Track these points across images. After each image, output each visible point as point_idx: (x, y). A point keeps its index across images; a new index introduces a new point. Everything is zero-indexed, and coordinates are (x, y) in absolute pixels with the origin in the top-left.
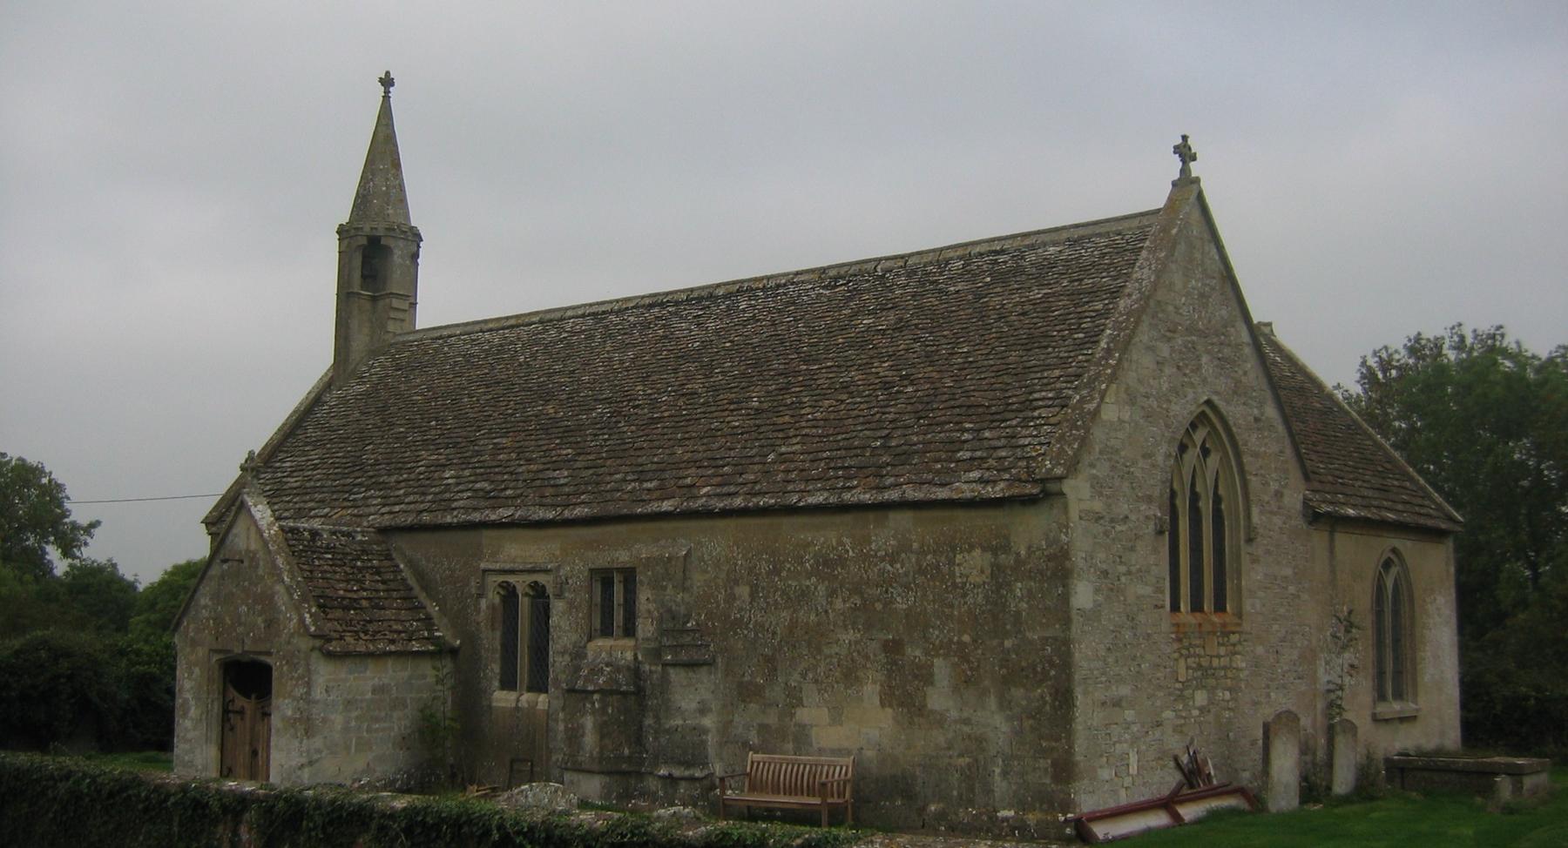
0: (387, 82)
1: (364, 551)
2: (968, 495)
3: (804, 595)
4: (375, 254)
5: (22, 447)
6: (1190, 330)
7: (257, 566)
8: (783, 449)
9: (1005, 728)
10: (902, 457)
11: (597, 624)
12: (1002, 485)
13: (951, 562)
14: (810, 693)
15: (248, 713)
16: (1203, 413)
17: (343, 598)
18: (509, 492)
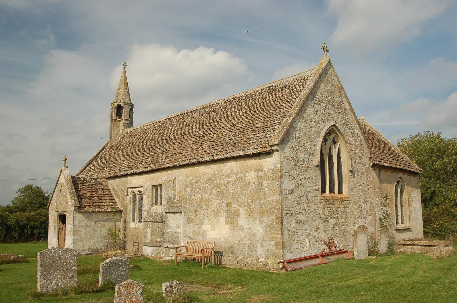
1: (100, 184)
2: (249, 153)
3: (205, 189)
4: (121, 111)
6: (327, 102)
8: (203, 146)
9: (261, 230)
10: (234, 144)
11: (154, 202)
12: (260, 149)
13: (245, 176)
14: (206, 220)
16: (333, 129)
17: (89, 196)
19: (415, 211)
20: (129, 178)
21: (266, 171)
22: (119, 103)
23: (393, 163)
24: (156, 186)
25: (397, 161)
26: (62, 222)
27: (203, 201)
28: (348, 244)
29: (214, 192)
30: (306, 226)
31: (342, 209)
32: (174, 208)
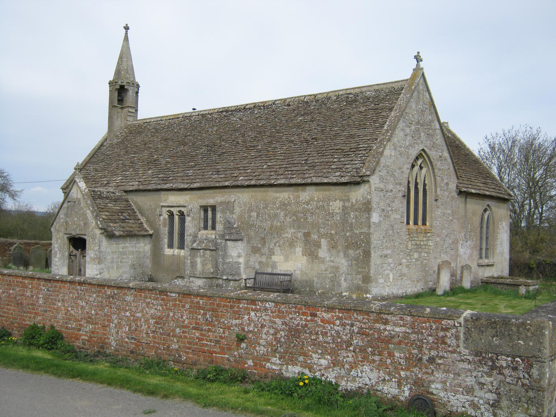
0: (127, 28)
3: (276, 216)
4: (122, 92)
7: (81, 204)
8: (270, 164)
11: (202, 225)
12: (347, 178)
13: (328, 205)
14: (277, 250)
15: (78, 256)
16: (421, 153)
18: (171, 178)
19: (501, 244)
20: (163, 194)
21: (354, 202)
22: (122, 84)
23: (482, 188)
24: (205, 209)
25: (485, 185)
26: (73, 247)
27: (273, 229)
28: (429, 280)
29: (288, 219)
30: (390, 260)
31: (425, 243)
32: (233, 234)
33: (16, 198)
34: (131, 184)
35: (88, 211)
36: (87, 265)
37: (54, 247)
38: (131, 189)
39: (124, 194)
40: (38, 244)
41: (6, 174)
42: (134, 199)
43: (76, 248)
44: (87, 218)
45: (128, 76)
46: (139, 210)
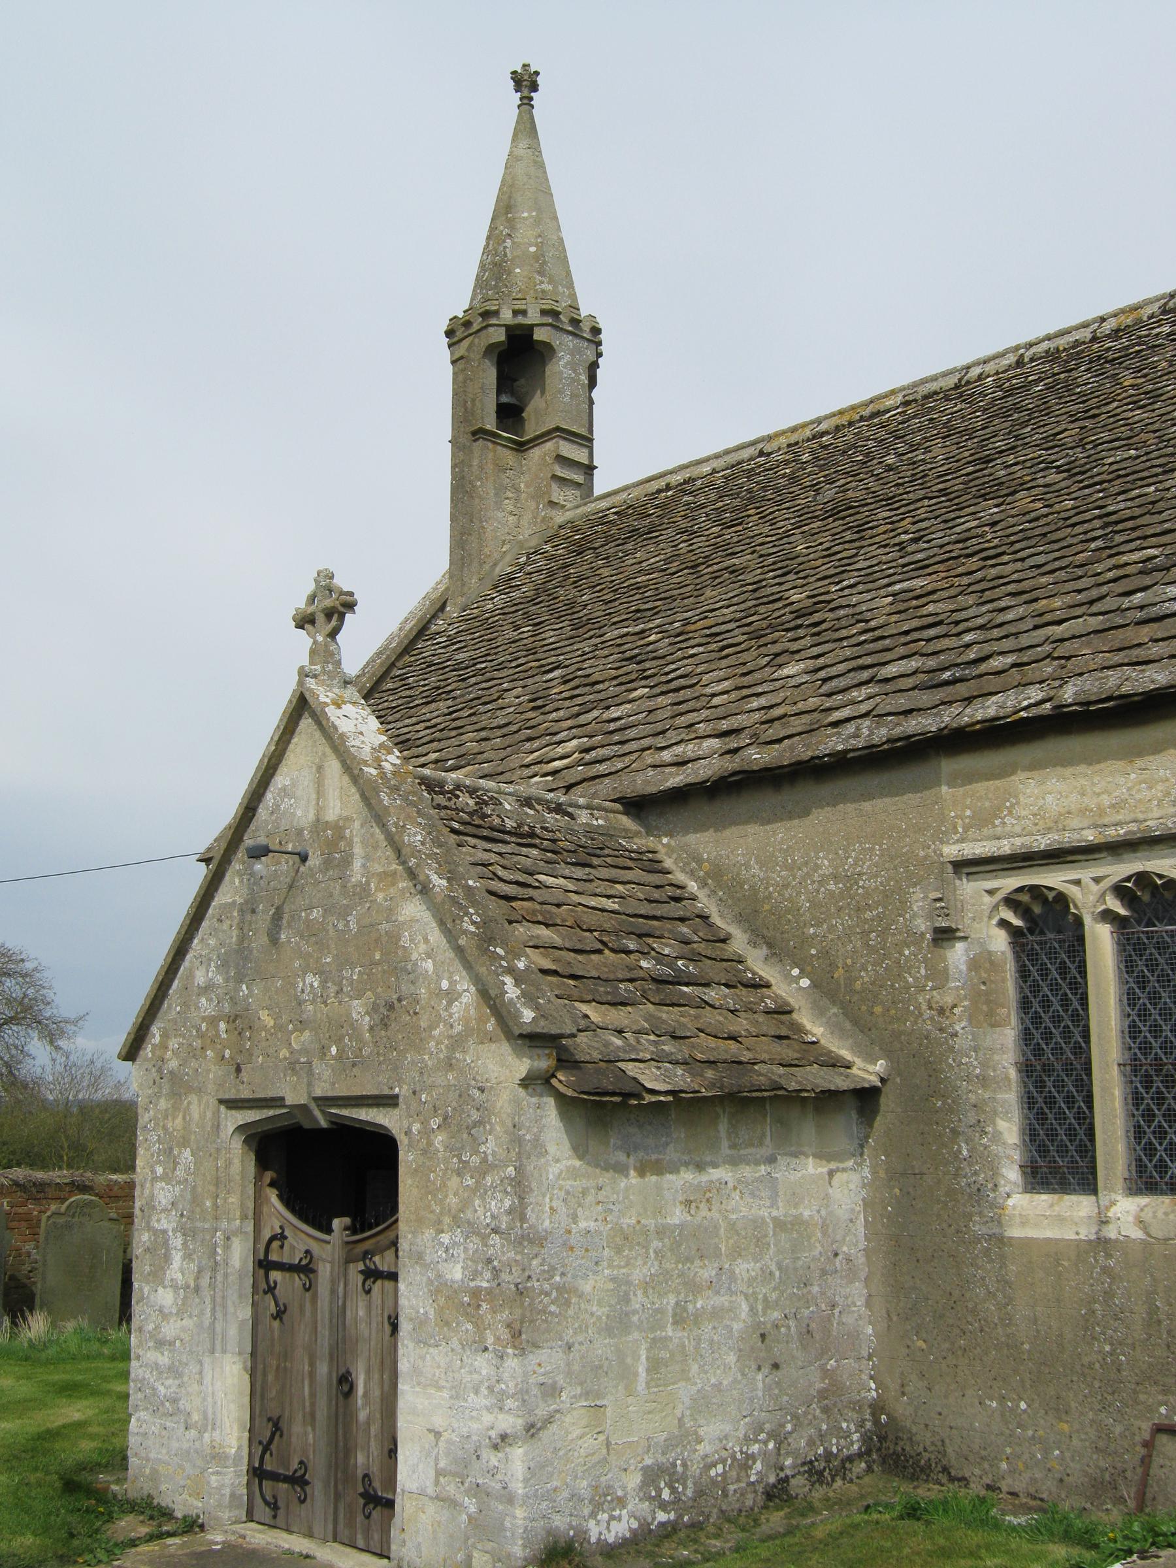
0: (526, 83)
4: (517, 363)
5: (13, 942)
7: (347, 861)
15: (325, 1271)
18: (997, 663)
22: (520, 320)
33: (60, 1043)
34: (666, 756)
35: (413, 910)
36: (408, 1354)
37: (150, 1206)
38: (676, 779)
39: (626, 821)
40: (84, 1188)
41: (29, 966)
42: (703, 858)
43: (310, 1206)
44: (398, 966)
45: (547, 287)
46: (749, 918)
